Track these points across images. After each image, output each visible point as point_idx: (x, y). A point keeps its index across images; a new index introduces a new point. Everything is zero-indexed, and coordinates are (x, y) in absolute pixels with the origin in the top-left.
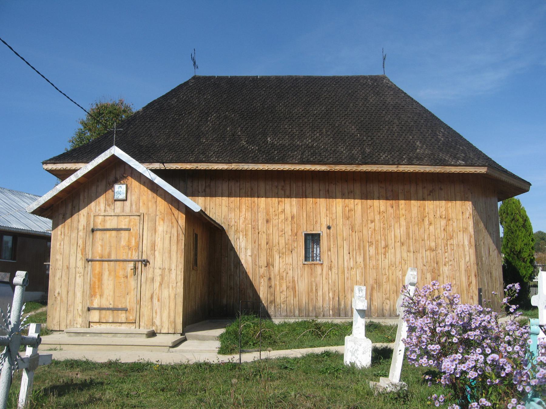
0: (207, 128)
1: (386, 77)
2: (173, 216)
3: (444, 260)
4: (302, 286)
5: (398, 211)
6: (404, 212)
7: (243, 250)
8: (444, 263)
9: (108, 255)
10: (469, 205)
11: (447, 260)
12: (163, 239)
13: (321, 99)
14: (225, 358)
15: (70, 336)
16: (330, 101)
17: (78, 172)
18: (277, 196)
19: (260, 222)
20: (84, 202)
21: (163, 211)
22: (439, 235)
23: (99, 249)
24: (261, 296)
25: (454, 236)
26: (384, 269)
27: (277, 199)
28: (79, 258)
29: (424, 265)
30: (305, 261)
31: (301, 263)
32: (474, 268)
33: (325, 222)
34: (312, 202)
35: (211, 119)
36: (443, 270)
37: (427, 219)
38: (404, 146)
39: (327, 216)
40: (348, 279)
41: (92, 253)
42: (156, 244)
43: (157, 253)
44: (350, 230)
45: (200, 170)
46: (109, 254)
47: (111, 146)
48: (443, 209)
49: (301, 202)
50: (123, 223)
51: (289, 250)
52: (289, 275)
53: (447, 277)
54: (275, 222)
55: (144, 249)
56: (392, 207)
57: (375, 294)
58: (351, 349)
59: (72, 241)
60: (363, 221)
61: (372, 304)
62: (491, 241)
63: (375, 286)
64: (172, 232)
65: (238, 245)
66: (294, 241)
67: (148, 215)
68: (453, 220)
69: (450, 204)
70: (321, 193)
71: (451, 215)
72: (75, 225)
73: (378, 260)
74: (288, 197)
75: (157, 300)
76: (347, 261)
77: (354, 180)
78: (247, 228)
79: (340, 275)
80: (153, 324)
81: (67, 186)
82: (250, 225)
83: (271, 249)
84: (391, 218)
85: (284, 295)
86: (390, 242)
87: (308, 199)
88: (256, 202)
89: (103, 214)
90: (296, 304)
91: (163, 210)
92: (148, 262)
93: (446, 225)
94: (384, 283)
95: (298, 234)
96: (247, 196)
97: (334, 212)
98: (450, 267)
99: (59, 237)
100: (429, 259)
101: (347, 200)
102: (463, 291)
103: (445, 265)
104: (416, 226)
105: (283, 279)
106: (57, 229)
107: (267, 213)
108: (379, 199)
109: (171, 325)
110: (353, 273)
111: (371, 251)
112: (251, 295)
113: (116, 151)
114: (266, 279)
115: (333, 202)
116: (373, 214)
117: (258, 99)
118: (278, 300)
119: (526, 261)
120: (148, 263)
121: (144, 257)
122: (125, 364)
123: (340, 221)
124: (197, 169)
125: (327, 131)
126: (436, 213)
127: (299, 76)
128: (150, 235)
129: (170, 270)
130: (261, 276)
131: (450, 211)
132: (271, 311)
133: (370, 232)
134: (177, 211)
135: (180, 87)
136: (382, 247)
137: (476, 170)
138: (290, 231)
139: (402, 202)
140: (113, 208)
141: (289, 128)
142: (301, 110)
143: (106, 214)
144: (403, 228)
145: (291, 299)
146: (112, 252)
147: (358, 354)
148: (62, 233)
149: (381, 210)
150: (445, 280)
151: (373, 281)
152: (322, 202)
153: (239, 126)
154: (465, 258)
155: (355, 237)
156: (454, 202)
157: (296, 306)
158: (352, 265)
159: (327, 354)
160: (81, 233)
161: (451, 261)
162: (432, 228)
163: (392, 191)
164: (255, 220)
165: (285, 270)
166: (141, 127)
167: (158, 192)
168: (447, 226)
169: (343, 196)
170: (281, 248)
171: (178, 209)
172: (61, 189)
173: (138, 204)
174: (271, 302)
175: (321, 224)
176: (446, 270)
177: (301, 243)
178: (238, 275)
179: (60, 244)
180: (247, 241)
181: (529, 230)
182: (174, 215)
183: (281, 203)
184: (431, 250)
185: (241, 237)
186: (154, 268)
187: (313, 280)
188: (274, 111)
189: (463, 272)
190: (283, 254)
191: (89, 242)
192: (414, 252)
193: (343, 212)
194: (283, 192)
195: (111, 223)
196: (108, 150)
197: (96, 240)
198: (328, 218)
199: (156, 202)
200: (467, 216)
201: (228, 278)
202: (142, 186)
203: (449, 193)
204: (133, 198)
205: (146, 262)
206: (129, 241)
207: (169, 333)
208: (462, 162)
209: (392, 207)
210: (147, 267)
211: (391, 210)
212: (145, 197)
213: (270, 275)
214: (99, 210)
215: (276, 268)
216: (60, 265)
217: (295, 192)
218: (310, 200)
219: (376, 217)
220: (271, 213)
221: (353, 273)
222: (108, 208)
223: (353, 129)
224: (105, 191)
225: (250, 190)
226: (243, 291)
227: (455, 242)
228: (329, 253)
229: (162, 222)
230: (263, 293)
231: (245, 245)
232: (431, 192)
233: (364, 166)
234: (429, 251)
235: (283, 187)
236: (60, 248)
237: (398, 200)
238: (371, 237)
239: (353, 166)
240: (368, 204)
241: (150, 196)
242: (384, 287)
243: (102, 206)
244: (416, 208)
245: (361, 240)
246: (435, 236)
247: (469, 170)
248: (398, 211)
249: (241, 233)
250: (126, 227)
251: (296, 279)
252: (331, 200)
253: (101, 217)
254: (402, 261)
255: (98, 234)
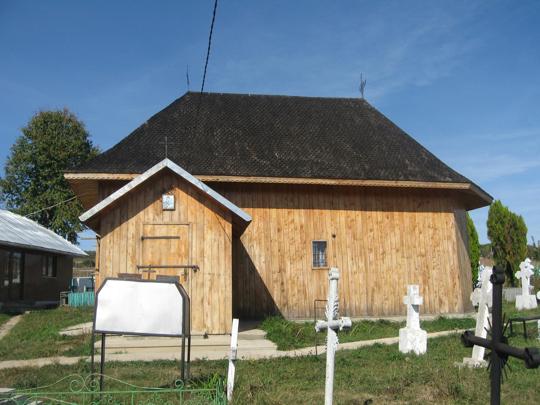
0: (216, 143)
1: (365, 101)
2: (220, 225)
3: (432, 264)
4: (312, 290)
5: (392, 221)
6: (398, 223)
7: (257, 257)
8: (432, 267)
9: (158, 262)
10: (451, 216)
11: (435, 264)
12: (212, 246)
13: (313, 119)
14: (283, 354)
15: (128, 340)
16: (321, 121)
17: (132, 183)
18: (287, 207)
19: (272, 231)
20: (132, 211)
21: (210, 221)
22: (428, 242)
23: (150, 257)
24: (275, 299)
25: (440, 243)
26: (383, 273)
27: (287, 210)
28: (129, 266)
29: (416, 269)
30: (314, 266)
31: (310, 268)
32: (457, 271)
33: (330, 231)
34: (318, 213)
35: (217, 134)
36: (432, 273)
37: (417, 229)
38: (396, 163)
39: (332, 226)
40: (352, 282)
41: (143, 260)
42: (205, 251)
43: (206, 259)
44: (353, 238)
45: (221, 182)
46: (160, 261)
47: (163, 158)
48: (430, 220)
49: (309, 213)
50: (173, 231)
51: (299, 256)
52: (299, 279)
53: (436, 279)
54: (286, 231)
55: (194, 256)
56: (388, 218)
57: (375, 295)
58: (411, 339)
59: (122, 249)
60: (363, 230)
61: (374, 304)
62: (465, 248)
63: (376, 288)
64: (220, 240)
65: (253, 252)
66: (303, 248)
67: (197, 224)
68: (439, 229)
69: (436, 215)
70: (326, 204)
71: (437, 225)
72: (124, 233)
73: (377, 265)
74: (297, 208)
75: (207, 303)
76: (351, 266)
77: (354, 193)
78: (260, 236)
79: (345, 279)
80: (204, 326)
81: (121, 195)
82: (263, 234)
83: (282, 256)
84: (387, 228)
85: (296, 298)
86: (387, 249)
87: (315, 210)
88: (268, 213)
89: (152, 222)
90: (307, 306)
91: (211, 219)
92: (198, 268)
93: (434, 234)
94: (383, 286)
95: (307, 242)
96: (259, 207)
97: (338, 222)
98: (438, 270)
99: (108, 245)
100: (420, 264)
101: (349, 211)
102: (449, 291)
103: (434, 269)
104: (408, 235)
105: (294, 283)
106: (105, 237)
107: (279, 223)
108: (376, 211)
109: (222, 327)
110: (356, 277)
111: (371, 257)
112: (266, 299)
113: (167, 163)
114: (279, 283)
115: (337, 213)
116: (371, 224)
117: (255, 116)
118: (290, 303)
119: (474, 266)
120: (198, 269)
121: (194, 264)
122: (213, 361)
123: (344, 230)
124: (218, 181)
125: (326, 149)
126: (425, 223)
127: (287, 96)
128: (198, 243)
129: (219, 275)
130: (274, 281)
131: (436, 222)
132: (285, 313)
133: (369, 240)
134: (224, 220)
135: (178, 102)
136: (380, 253)
137: (461, 186)
138: (299, 239)
139: (396, 214)
140: (162, 217)
141: (292, 145)
142: (297, 128)
143: (155, 222)
144: (398, 237)
145: (302, 301)
146: (163, 259)
147: (416, 343)
148: (110, 241)
149: (379, 220)
150: (434, 282)
151: (374, 284)
152: (327, 213)
153: (246, 141)
154: (450, 263)
155: (358, 244)
156: (439, 213)
157: (307, 308)
158: (355, 270)
159: (377, 345)
160: (130, 241)
161: (438, 265)
162: (421, 236)
163: (387, 203)
164: (268, 229)
165: (296, 275)
166: (151, 139)
167: (205, 202)
168: (435, 235)
169: (346, 208)
170: (292, 255)
171: (225, 219)
172: (115, 199)
173: (185, 214)
174: (284, 305)
175: (327, 233)
176: (434, 273)
177: (310, 251)
178: (254, 281)
179: (109, 251)
180: (261, 248)
181: (476, 239)
182: (221, 224)
183: (290, 214)
184: (422, 256)
185: (255, 245)
186: (203, 274)
187: (321, 283)
188: (273, 128)
189: (449, 274)
190: (294, 260)
191: (139, 251)
192: (407, 258)
193: (346, 222)
194: (292, 204)
195: (161, 231)
196: (161, 162)
197: (146, 248)
198: (333, 228)
199: (204, 211)
200: (451, 226)
201: (244, 284)
202: (190, 197)
203: (435, 206)
204: (181, 207)
205: (195, 269)
206: (179, 249)
207: (219, 334)
208: (449, 179)
209: (388, 218)
210: (197, 272)
211: (387, 221)
212: (192, 207)
213: (282, 280)
214: (148, 219)
215: (288, 274)
216: (110, 272)
217: (302, 204)
218: (317, 211)
219: (374, 226)
220: (282, 223)
221: (356, 277)
222: (157, 217)
223: (349, 147)
224: (154, 201)
225: (262, 201)
226: (258, 295)
227: (441, 248)
228: (335, 259)
229: (209, 231)
230: (276, 296)
231: (259, 252)
232: (420, 204)
233: (368, 181)
234: (420, 257)
235: (292, 198)
236: (109, 256)
237: (393, 211)
238: (371, 245)
239: (358, 181)
240: (367, 215)
241: (198, 206)
242: (383, 288)
243: (151, 216)
244: (408, 219)
245: (362, 247)
246: (424, 243)
247: (456, 186)
248: (392, 221)
249: (255, 241)
250: (176, 235)
251: (306, 283)
252: (335, 211)
253: (150, 226)
254: (398, 265)
255: (148, 242)
